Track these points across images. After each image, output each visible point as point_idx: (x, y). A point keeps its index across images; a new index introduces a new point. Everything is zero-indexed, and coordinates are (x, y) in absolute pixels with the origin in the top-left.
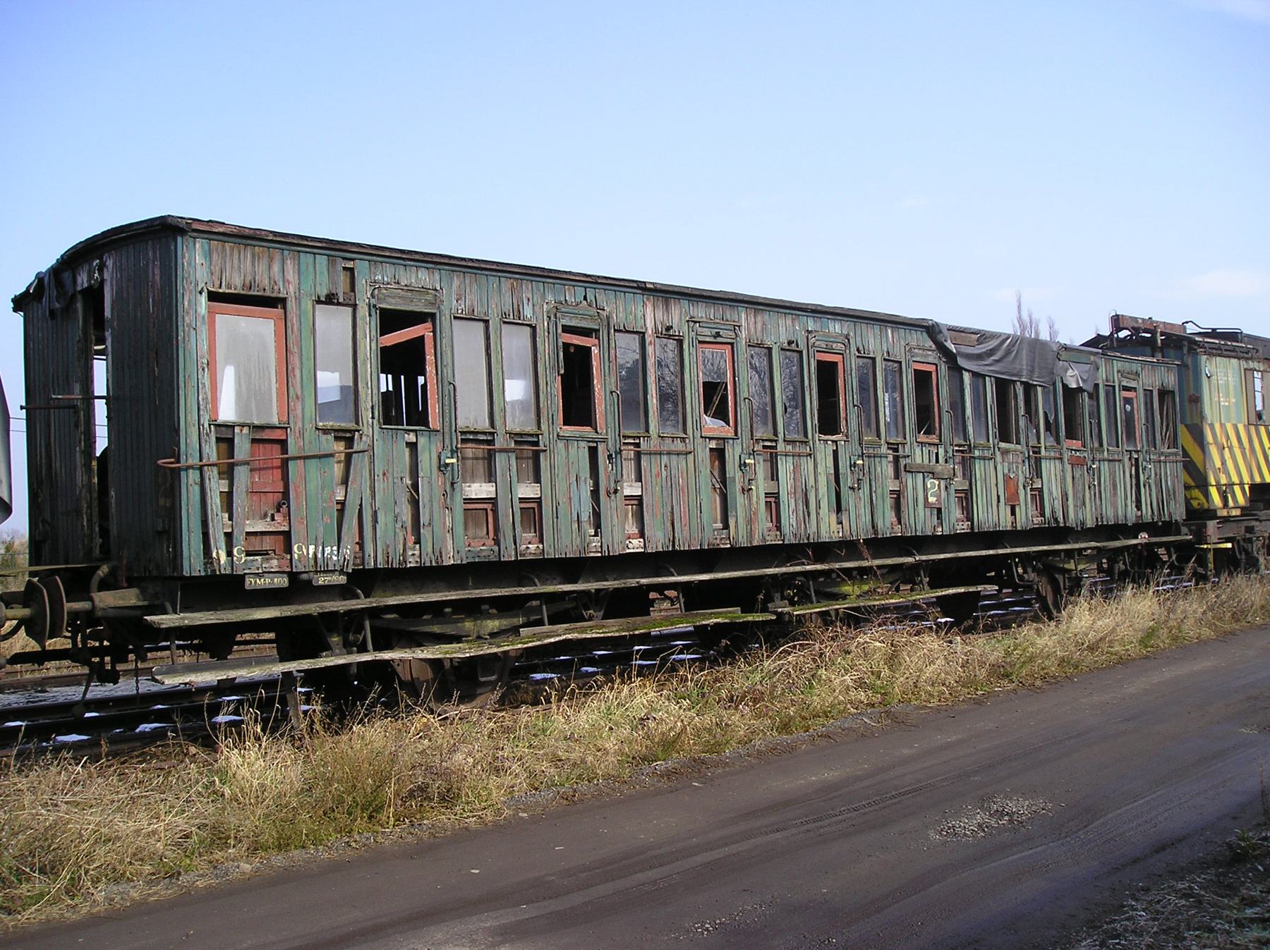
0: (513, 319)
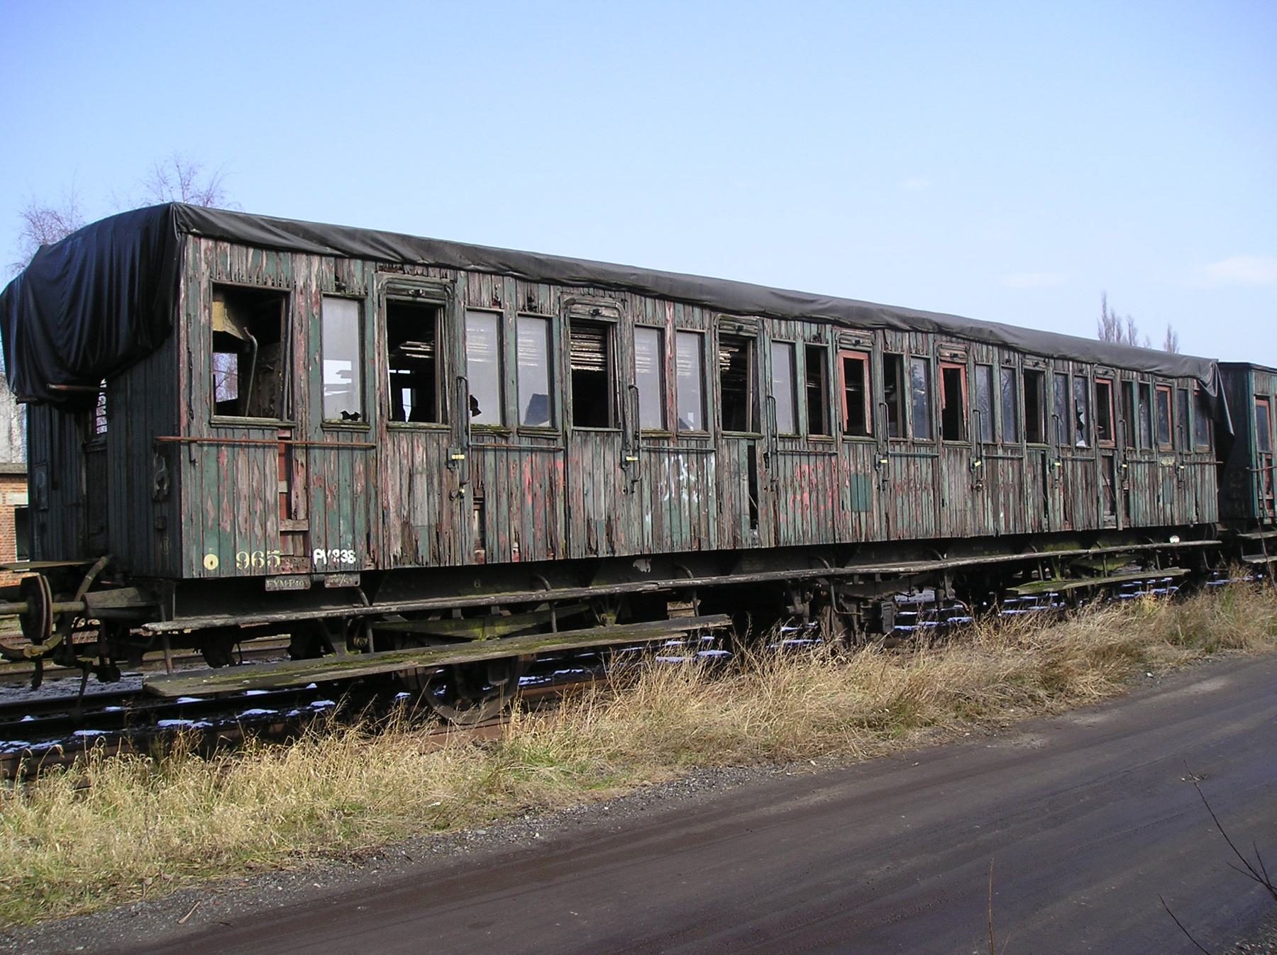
0: (530, 309)
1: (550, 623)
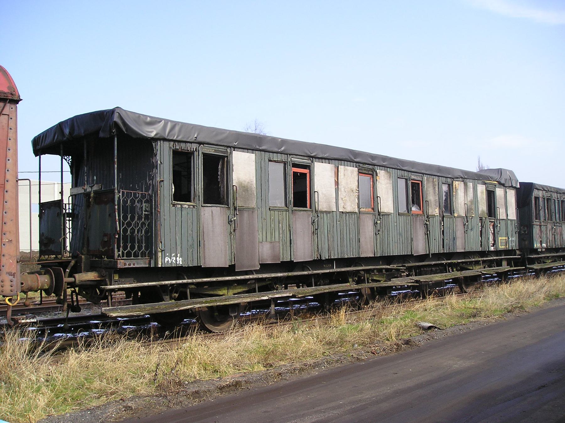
1: (255, 289)
